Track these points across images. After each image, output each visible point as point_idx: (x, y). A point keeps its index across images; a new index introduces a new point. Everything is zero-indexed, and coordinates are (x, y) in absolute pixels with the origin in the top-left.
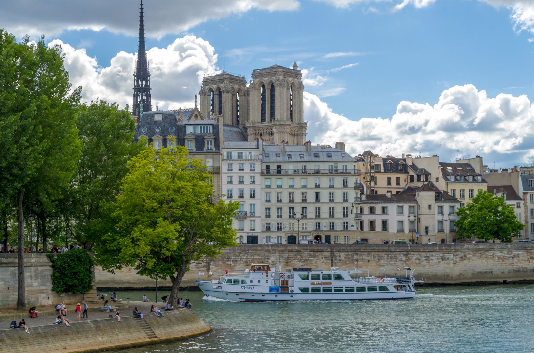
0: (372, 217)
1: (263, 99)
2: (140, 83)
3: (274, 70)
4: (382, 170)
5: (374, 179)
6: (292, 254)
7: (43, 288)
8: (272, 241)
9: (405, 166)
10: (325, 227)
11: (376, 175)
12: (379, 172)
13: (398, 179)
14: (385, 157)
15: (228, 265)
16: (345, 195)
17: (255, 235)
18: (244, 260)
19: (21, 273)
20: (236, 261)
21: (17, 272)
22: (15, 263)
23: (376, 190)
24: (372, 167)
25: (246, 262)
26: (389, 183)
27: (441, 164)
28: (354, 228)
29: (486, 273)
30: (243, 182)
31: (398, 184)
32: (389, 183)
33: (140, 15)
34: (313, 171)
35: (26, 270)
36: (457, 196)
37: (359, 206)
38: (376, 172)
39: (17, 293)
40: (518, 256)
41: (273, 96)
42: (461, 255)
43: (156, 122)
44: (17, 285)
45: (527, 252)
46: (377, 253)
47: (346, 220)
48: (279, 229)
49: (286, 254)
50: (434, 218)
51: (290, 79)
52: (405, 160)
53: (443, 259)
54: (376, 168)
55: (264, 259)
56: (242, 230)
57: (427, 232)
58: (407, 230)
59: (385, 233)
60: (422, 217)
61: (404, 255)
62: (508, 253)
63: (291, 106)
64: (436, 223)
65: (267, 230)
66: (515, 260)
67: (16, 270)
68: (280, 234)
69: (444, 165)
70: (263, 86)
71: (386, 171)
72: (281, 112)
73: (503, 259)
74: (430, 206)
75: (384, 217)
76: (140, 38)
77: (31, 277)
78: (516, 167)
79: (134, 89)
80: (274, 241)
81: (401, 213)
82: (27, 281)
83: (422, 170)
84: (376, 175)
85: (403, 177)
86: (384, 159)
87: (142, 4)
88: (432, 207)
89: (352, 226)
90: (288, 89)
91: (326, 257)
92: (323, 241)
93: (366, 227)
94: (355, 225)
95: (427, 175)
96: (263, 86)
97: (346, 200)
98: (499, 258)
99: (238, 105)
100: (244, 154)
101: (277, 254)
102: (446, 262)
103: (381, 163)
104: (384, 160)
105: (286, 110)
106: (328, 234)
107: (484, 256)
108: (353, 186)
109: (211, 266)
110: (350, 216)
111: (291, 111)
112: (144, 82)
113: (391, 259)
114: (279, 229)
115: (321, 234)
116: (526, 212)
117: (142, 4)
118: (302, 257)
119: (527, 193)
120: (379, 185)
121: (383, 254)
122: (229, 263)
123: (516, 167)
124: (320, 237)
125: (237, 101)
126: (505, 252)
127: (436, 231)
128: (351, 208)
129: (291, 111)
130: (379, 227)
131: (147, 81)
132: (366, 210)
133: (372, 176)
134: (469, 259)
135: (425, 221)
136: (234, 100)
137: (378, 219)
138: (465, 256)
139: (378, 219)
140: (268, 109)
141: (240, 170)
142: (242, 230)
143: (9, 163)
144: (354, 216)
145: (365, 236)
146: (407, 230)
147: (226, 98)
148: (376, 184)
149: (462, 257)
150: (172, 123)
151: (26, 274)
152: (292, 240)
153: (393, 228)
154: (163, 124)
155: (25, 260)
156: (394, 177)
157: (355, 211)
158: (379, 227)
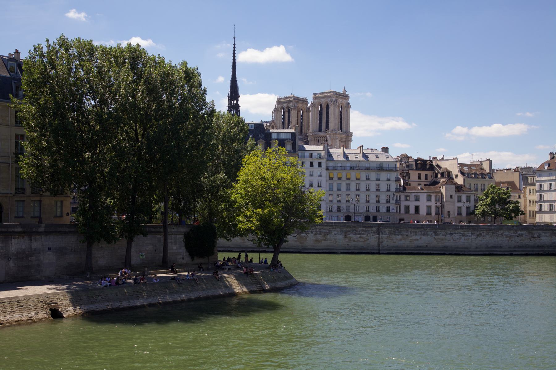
0: (407, 203)
1: (321, 115)
3: (327, 95)
4: (415, 168)
5: (408, 175)
6: (349, 229)
7: (181, 251)
8: (333, 218)
9: (431, 165)
10: (373, 209)
11: (410, 172)
12: (412, 169)
13: (426, 175)
14: (416, 158)
16: (388, 186)
19: (165, 240)
21: (162, 239)
22: (161, 232)
23: (409, 182)
24: (407, 166)
26: (419, 178)
27: (459, 164)
28: (395, 211)
29: (496, 247)
30: (312, 175)
31: (426, 178)
32: (419, 178)
34: (365, 168)
35: (169, 237)
36: (473, 188)
37: (398, 195)
38: (410, 170)
39: (162, 255)
40: (522, 235)
41: (327, 113)
42: (478, 233)
44: (162, 248)
45: (529, 233)
46: (413, 230)
47: (388, 205)
48: (339, 210)
49: (345, 229)
50: (454, 205)
51: (341, 100)
52: (431, 161)
53: (463, 235)
54: (410, 167)
57: (449, 216)
58: (433, 213)
59: (417, 215)
60: (446, 204)
61: (434, 232)
62: (514, 233)
63: (341, 120)
64: (456, 209)
65: (330, 211)
66: (520, 238)
67: (161, 237)
68: (339, 214)
69: (462, 165)
70: (321, 105)
71: (417, 169)
72: (333, 123)
73: (510, 237)
74: (451, 197)
75: (417, 203)
76: (233, 69)
77: (172, 243)
78: (517, 167)
79: (228, 106)
80: (334, 219)
81: (429, 200)
82: (169, 245)
83: (445, 169)
84: (410, 172)
85: (429, 173)
86: (415, 160)
87: (234, 45)
88: (453, 197)
89: (393, 209)
90: (339, 108)
91: (374, 232)
92: (371, 220)
93: (403, 210)
94: (395, 209)
95: (449, 173)
96: (321, 105)
97: (388, 190)
98: (507, 236)
99: (302, 119)
100: (314, 154)
101: (338, 229)
102: (466, 238)
103: (414, 163)
104: (416, 161)
105: (337, 123)
106: (375, 215)
107: (495, 235)
108: (394, 179)
110: (392, 201)
111: (341, 124)
112: (235, 102)
113: (424, 234)
114: (339, 210)
115: (370, 215)
116: (525, 202)
117: (234, 45)
118: (357, 231)
119: (526, 187)
120: (412, 179)
121: (417, 231)
123: (517, 167)
124: (369, 217)
125: (301, 116)
126: (512, 232)
127: (456, 214)
128: (392, 196)
129: (341, 124)
130: (412, 210)
131: (237, 100)
132: (403, 198)
133: (407, 173)
134: (484, 236)
135: (447, 208)
136: (299, 116)
137: (412, 205)
138: (481, 234)
139: (412, 205)
140: (323, 123)
143: (119, 164)
144: (394, 202)
145: (402, 217)
146: (433, 213)
147: (293, 113)
148: (409, 178)
149: (478, 235)
150: (260, 132)
151: (169, 241)
152: (348, 218)
153: (423, 211)
155: (169, 230)
156: (423, 173)
157: (395, 198)
158: (412, 210)
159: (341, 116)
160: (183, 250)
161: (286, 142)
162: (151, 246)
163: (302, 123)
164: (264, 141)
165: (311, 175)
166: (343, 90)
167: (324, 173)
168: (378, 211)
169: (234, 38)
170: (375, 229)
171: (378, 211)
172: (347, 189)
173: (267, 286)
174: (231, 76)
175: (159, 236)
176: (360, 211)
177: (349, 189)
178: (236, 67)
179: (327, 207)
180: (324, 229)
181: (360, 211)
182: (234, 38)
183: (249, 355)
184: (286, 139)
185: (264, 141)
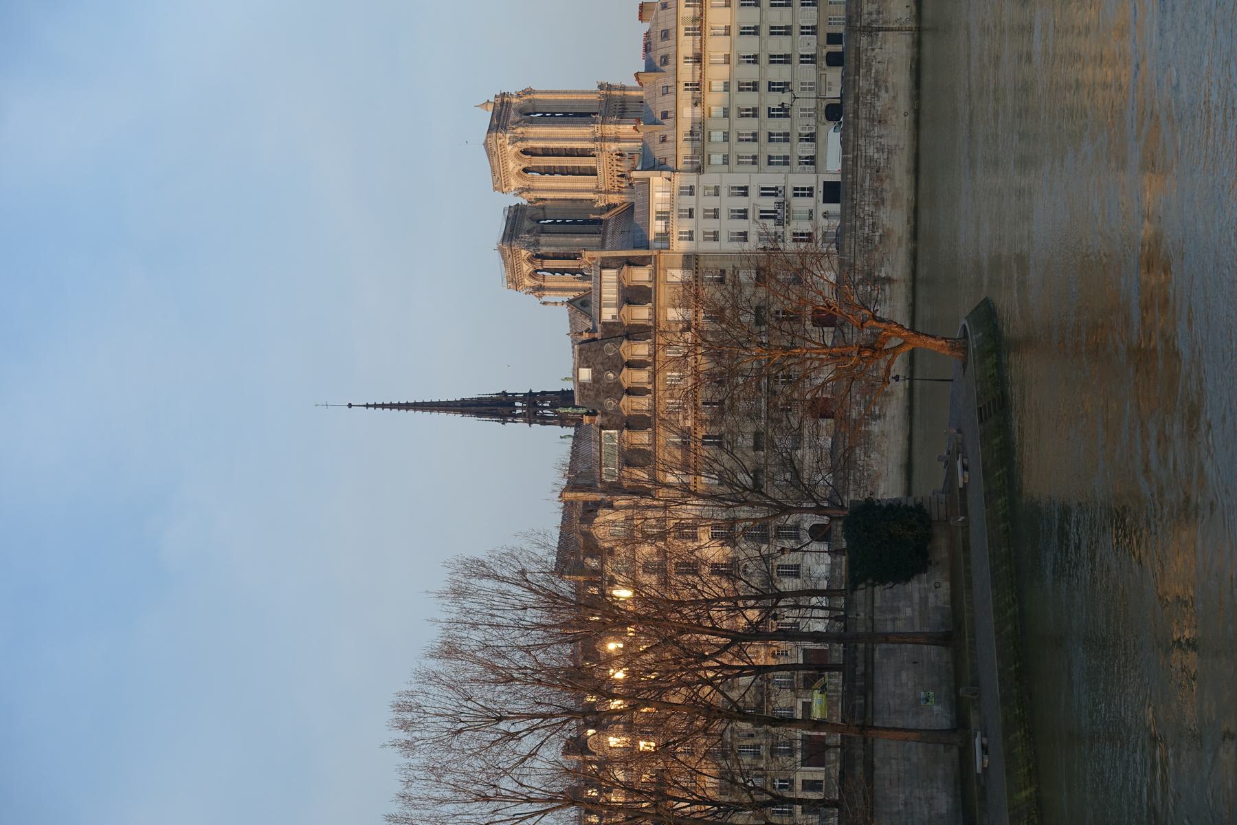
2: (519, 411)
6: (863, 112)
7: (916, 596)
15: (881, 242)
17: (821, 188)
18: (872, 209)
19: (886, 638)
20: (874, 224)
25: (876, 205)
33: (387, 410)
41: (547, 152)
43: (596, 380)
44: (910, 646)
49: (863, 124)
55: (872, 168)
56: (811, 212)
77: (894, 620)
82: (901, 626)
87: (367, 406)
91: (871, 43)
92: (839, 48)
96: (526, 170)
99: (564, 222)
106: (824, 39)
109: (883, 275)
114: (811, 138)
115: (825, 52)
117: (367, 406)
118: (869, 91)
122: (877, 238)
124: (829, 54)
125: (554, 222)
141: (691, 216)
142: (811, 212)
154: (599, 367)
159: (553, 114)
160: (914, 588)
161: (626, 285)
162: (904, 675)
163: (575, 222)
164: (625, 343)
165: (716, 214)
166: (483, 111)
167: (709, 179)
168: (813, 30)
169: (350, 406)
170: (864, 41)
171: (813, 30)
172: (754, 116)
173: (608, 524)
174: (451, 415)
175: (877, 655)
176: (814, 80)
177: (755, 110)
178: (419, 401)
179: (803, 172)
180: (863, 181)
181: (814, 80)
182: (350, 406)
183: (649, 507)
184: (619, 282)
185: (625, 343)
